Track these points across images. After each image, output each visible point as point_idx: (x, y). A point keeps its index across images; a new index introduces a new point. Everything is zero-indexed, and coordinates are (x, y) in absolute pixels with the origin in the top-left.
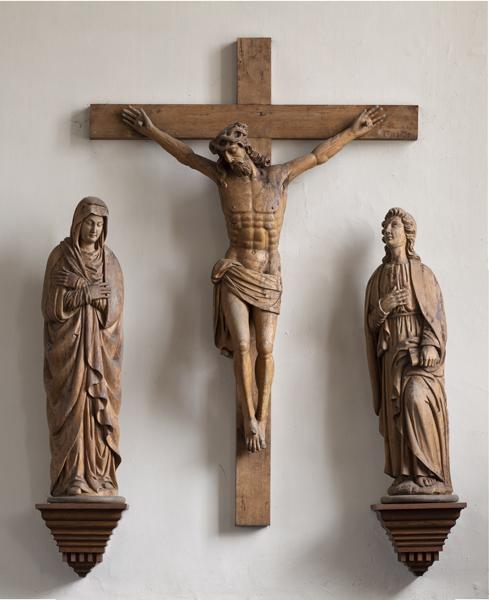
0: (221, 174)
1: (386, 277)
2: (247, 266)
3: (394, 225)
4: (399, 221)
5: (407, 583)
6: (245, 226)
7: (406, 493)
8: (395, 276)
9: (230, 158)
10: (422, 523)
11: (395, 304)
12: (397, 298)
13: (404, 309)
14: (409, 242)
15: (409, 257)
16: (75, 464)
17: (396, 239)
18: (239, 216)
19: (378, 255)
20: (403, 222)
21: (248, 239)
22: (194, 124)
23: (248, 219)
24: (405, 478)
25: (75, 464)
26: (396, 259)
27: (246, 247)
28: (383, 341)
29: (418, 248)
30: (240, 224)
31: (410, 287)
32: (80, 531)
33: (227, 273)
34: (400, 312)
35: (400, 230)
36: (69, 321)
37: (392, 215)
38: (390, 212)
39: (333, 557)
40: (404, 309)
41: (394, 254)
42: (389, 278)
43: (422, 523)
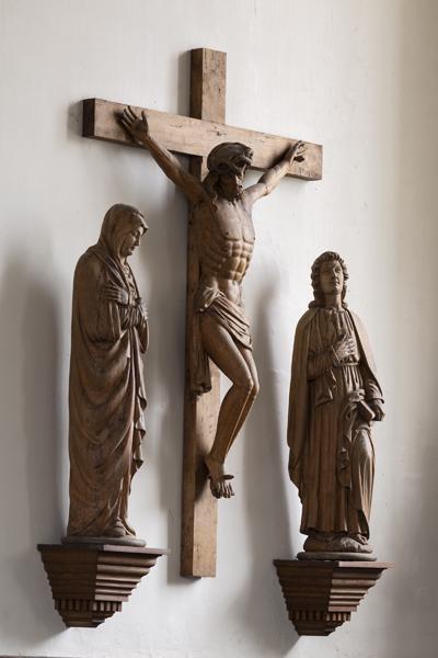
0: (213, 197)
2: (228, 296)
5: (59, 631)
6: (234, 255)
7: (353, 550)
10: (354, 582)
11: (347, 354)
18: (231, 243)
21: (233, 269)
22: (171, 135)
23: (239, 247)
24: (346, 534)
27: (228, 276)
28: (331, 394)
30: (231, 251)
32: (82, 576)
33: (215, 303)
39: (248, 614)
42: (335, 324)
43: (354, 582)
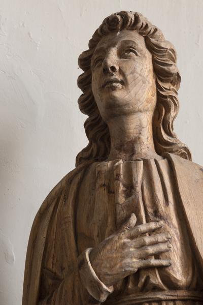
1: (102, 193)
3: (126, 51)
4: (140, 43)
8: (130, 188)
9: (113, 58)
11: (134, 263)
12: (143, 246)
13: (157, 280)
14: (163, 107)
15: (162, 147)
16: (196, 269)
17: (133, 90)
19: (63, 141)
20: (151, 47)
25: (196, 269)
26: (129, 148)
29: (183, 128)
31: (175, 221)
34: (149, 287)
35: (142, 66)
36: (107, 233)
37: (115, 28)
38: (180, 77)
40: (157, 280)
41: (123, 131)
